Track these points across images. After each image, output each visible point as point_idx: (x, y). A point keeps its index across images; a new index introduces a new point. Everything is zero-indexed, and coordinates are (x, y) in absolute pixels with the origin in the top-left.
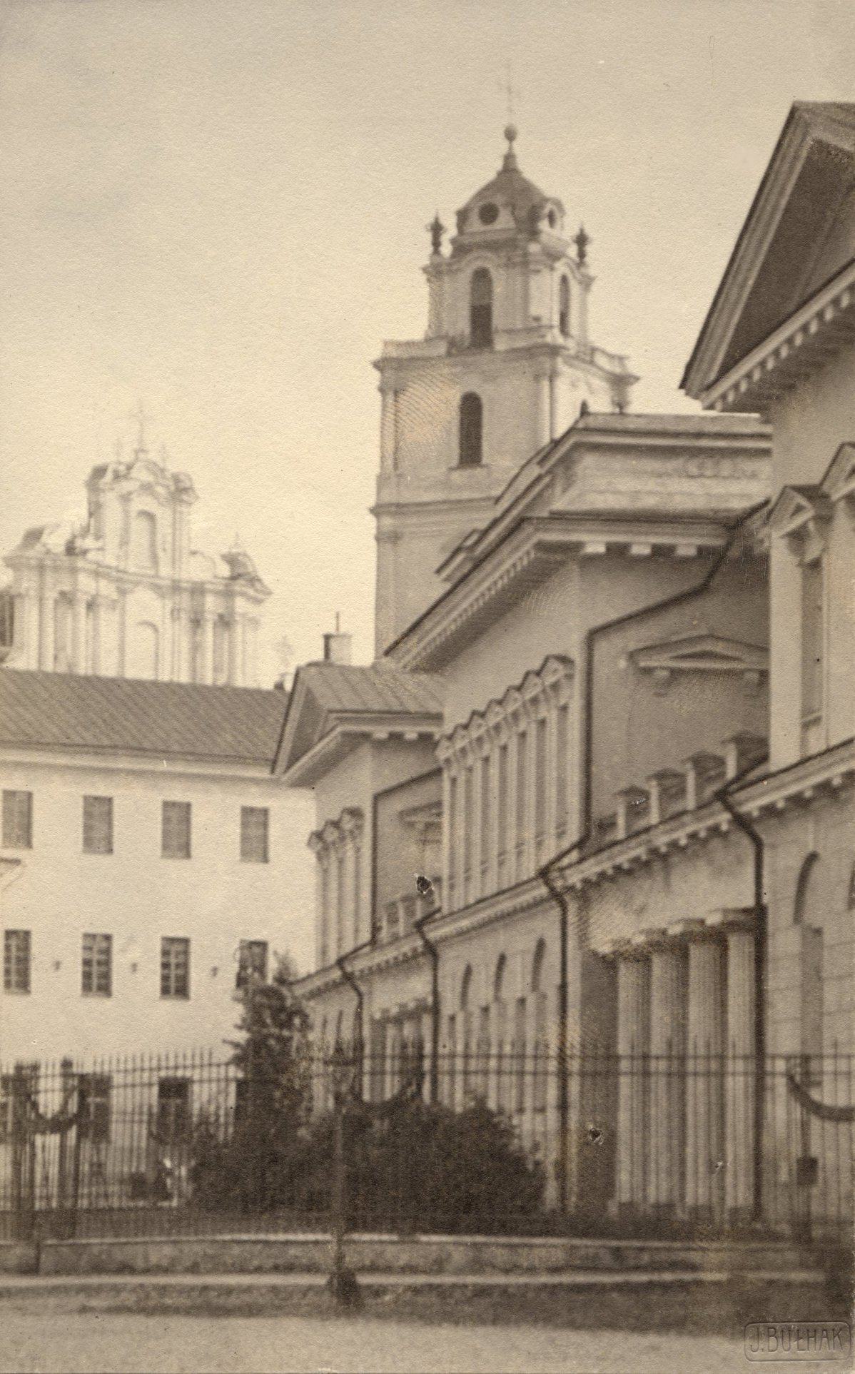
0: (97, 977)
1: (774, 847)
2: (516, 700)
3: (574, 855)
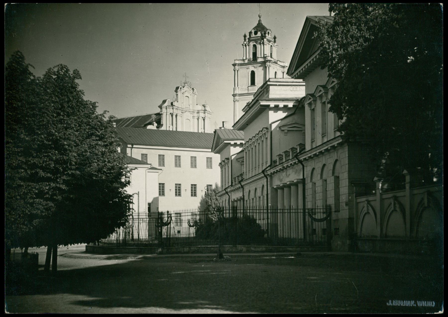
0: (178, 192)
3: (269, 168)
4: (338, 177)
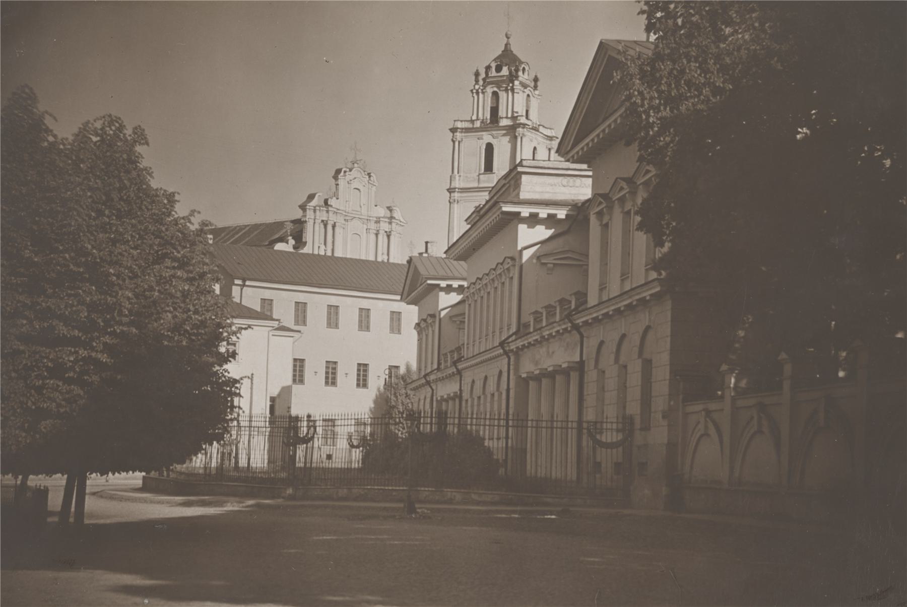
0: (331, 378)
3: (514, 337)
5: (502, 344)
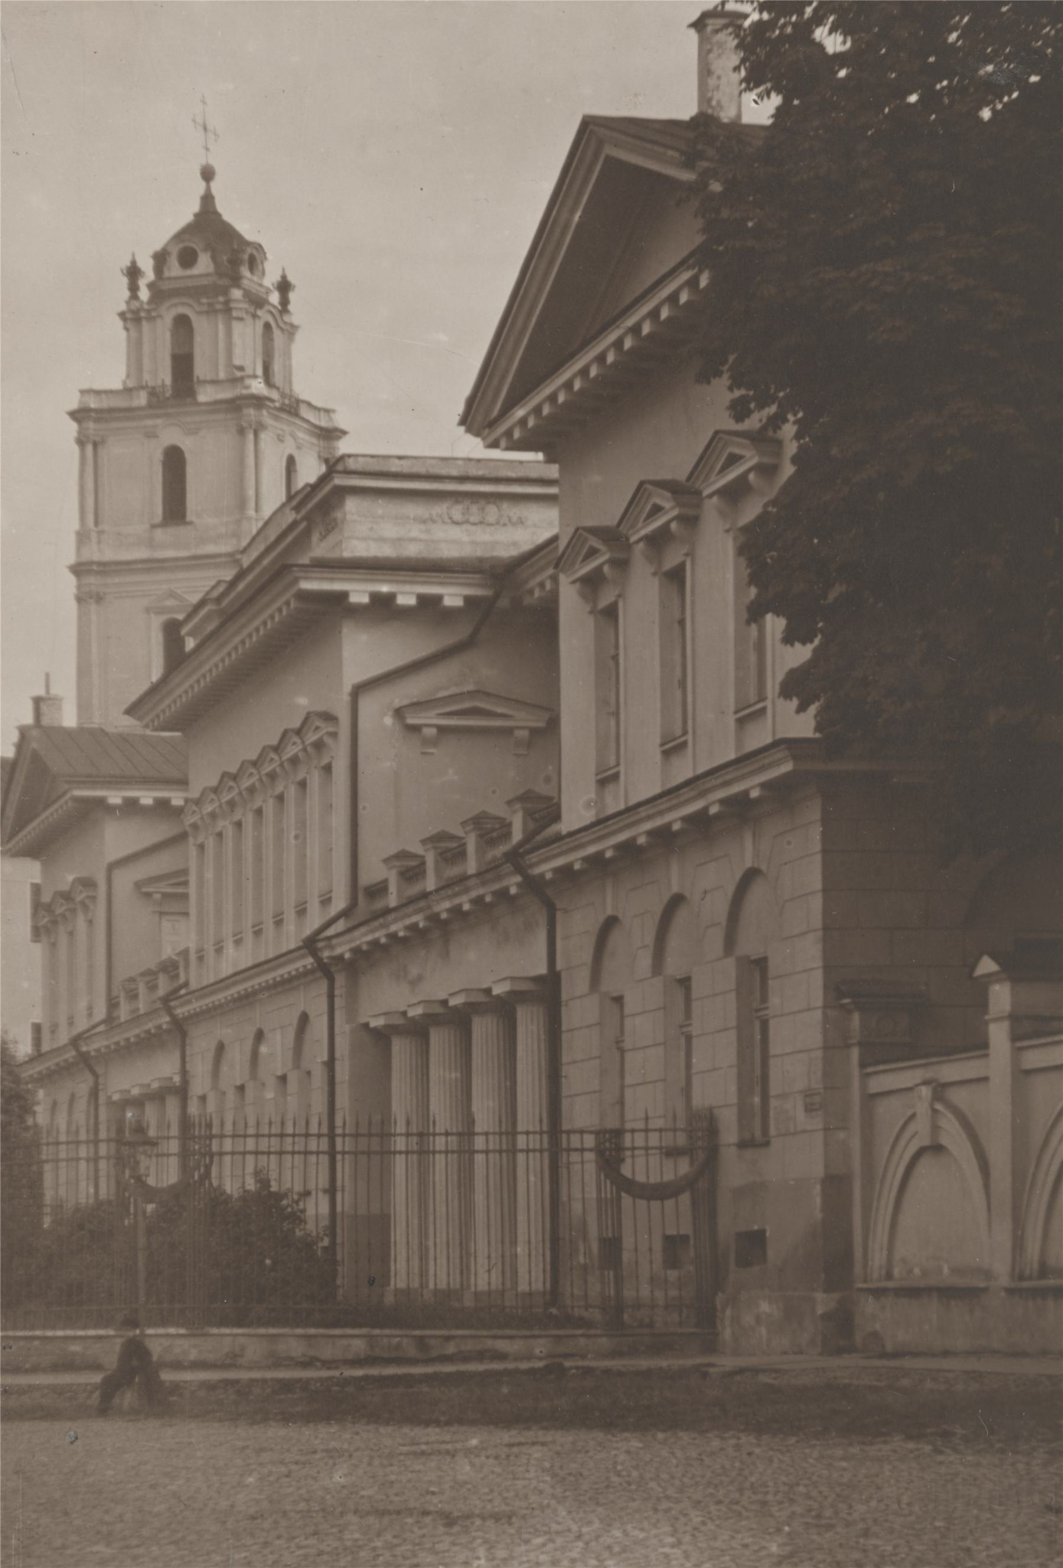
1: (566, 911)
2: (272, 760)
3: (340, 926)
4: (761, 964)
5: (310, 944)
